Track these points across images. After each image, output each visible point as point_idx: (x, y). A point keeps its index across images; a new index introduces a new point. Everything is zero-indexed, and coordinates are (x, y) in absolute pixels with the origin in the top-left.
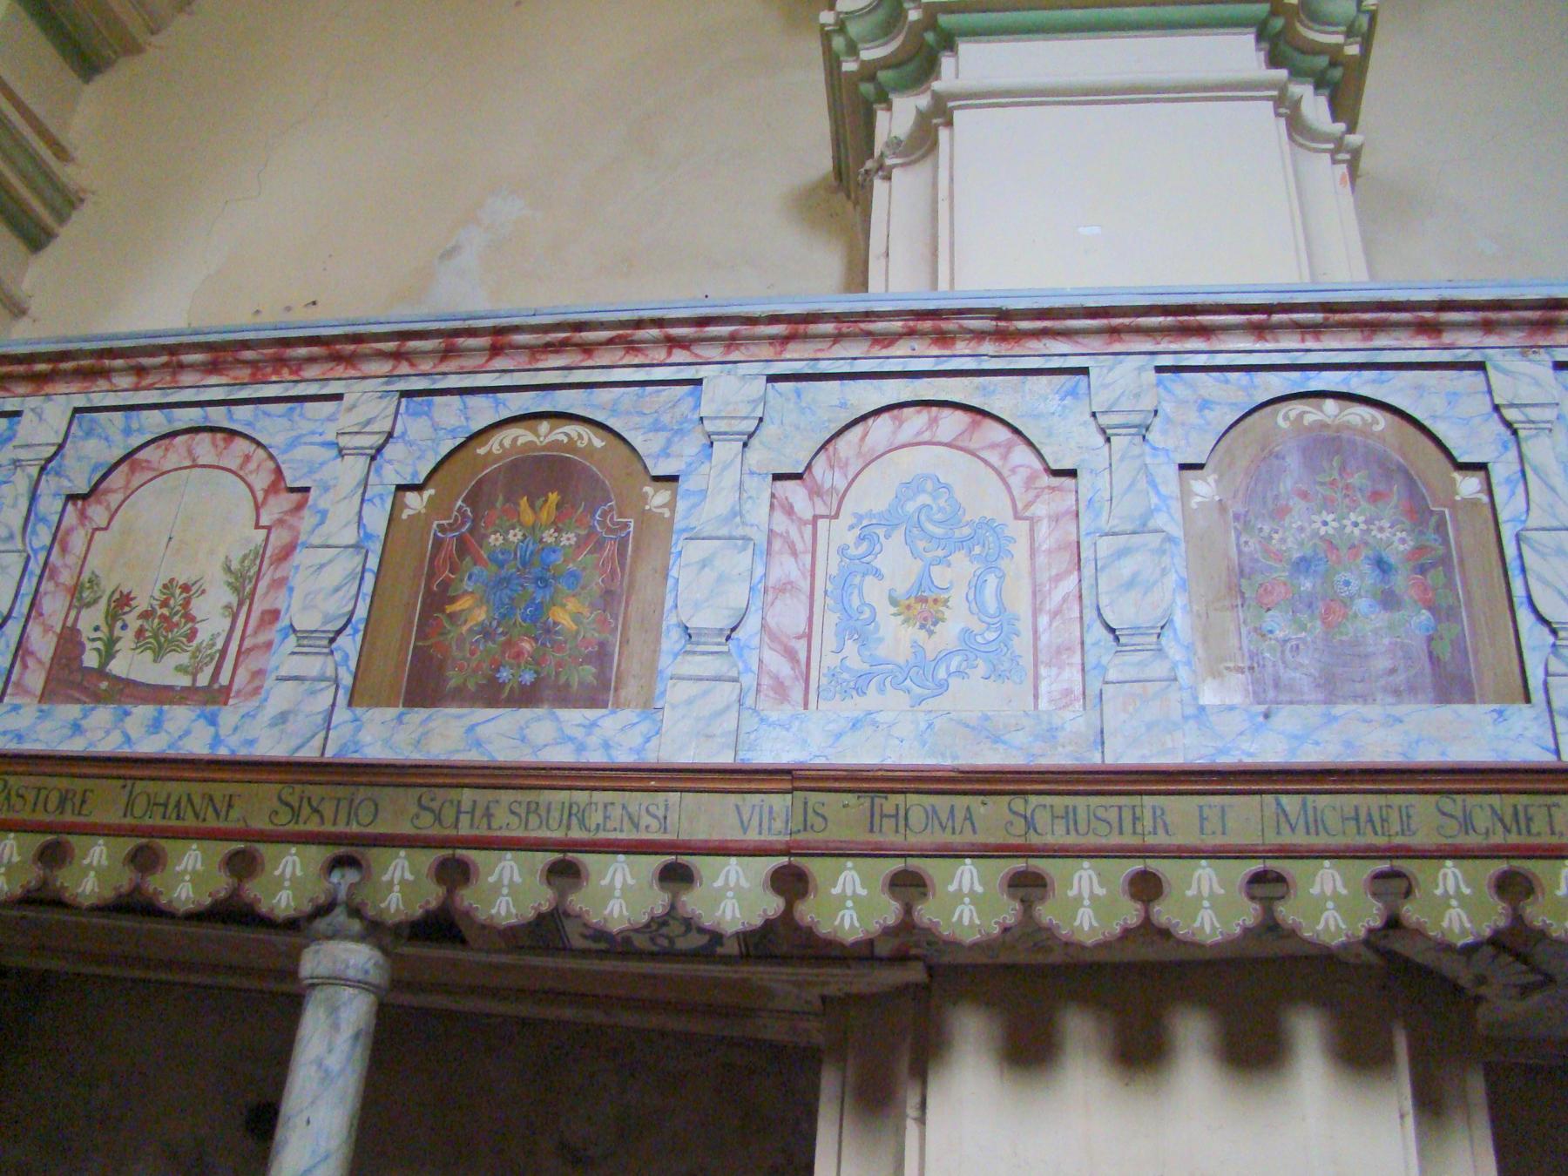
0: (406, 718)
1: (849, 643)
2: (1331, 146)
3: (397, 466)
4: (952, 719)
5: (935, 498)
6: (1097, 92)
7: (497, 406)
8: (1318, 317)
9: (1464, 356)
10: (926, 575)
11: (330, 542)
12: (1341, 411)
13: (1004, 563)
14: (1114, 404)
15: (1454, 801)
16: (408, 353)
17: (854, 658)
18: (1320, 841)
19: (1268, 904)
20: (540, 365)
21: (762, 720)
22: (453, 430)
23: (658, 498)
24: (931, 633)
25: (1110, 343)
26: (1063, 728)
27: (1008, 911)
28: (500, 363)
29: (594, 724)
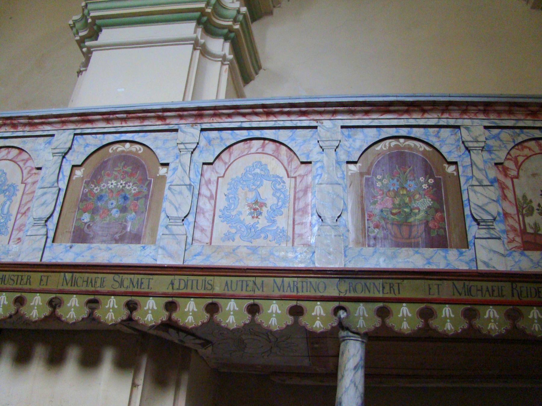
2: (221, 59)
6: (151, 43)
8: (124, 116)
12: (131, 146)
14: (58, 146)
15: (119, 276)
18: (75, 288)
19: (92, 310)
23: (162, 171)
27: (247, 318)
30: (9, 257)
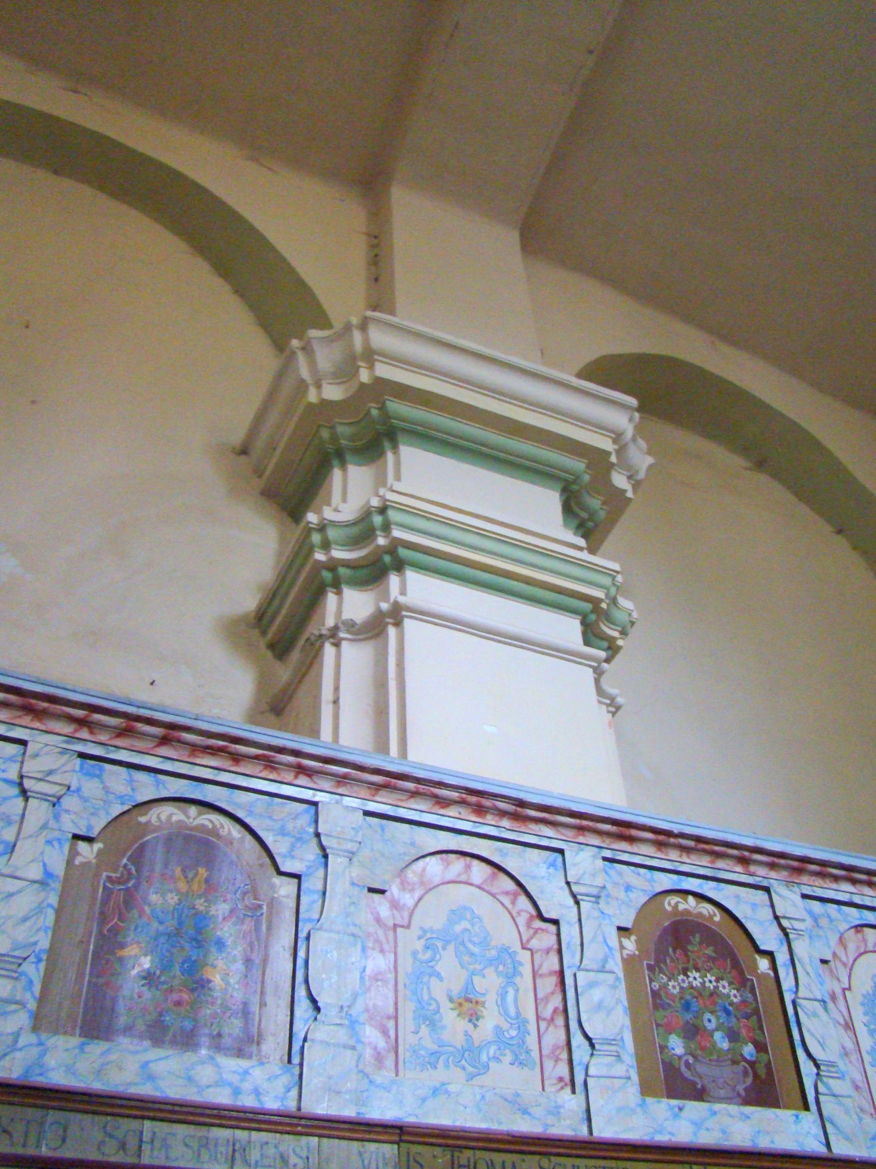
0: (88, 1048)
1: (423, 1026)
3: (73, 817)
4: (496, 1094)
5: (473, 925)
7: (158, 786)
8: (692, 843)
9: (760, 882)
10: (470, 982)
11: (17, 874)
13: (517, 980)
15: (550, 1160)
16: (92, 723)
17: (426, 1039)
20: (198, 761)
21: (371, 1082)
22: (122, 797)
24: (475, 1026)
25: (578, 835)
26: (564, 1107)
28: (164, 751)
29: (246, 1072)
30: (563, 1122)
